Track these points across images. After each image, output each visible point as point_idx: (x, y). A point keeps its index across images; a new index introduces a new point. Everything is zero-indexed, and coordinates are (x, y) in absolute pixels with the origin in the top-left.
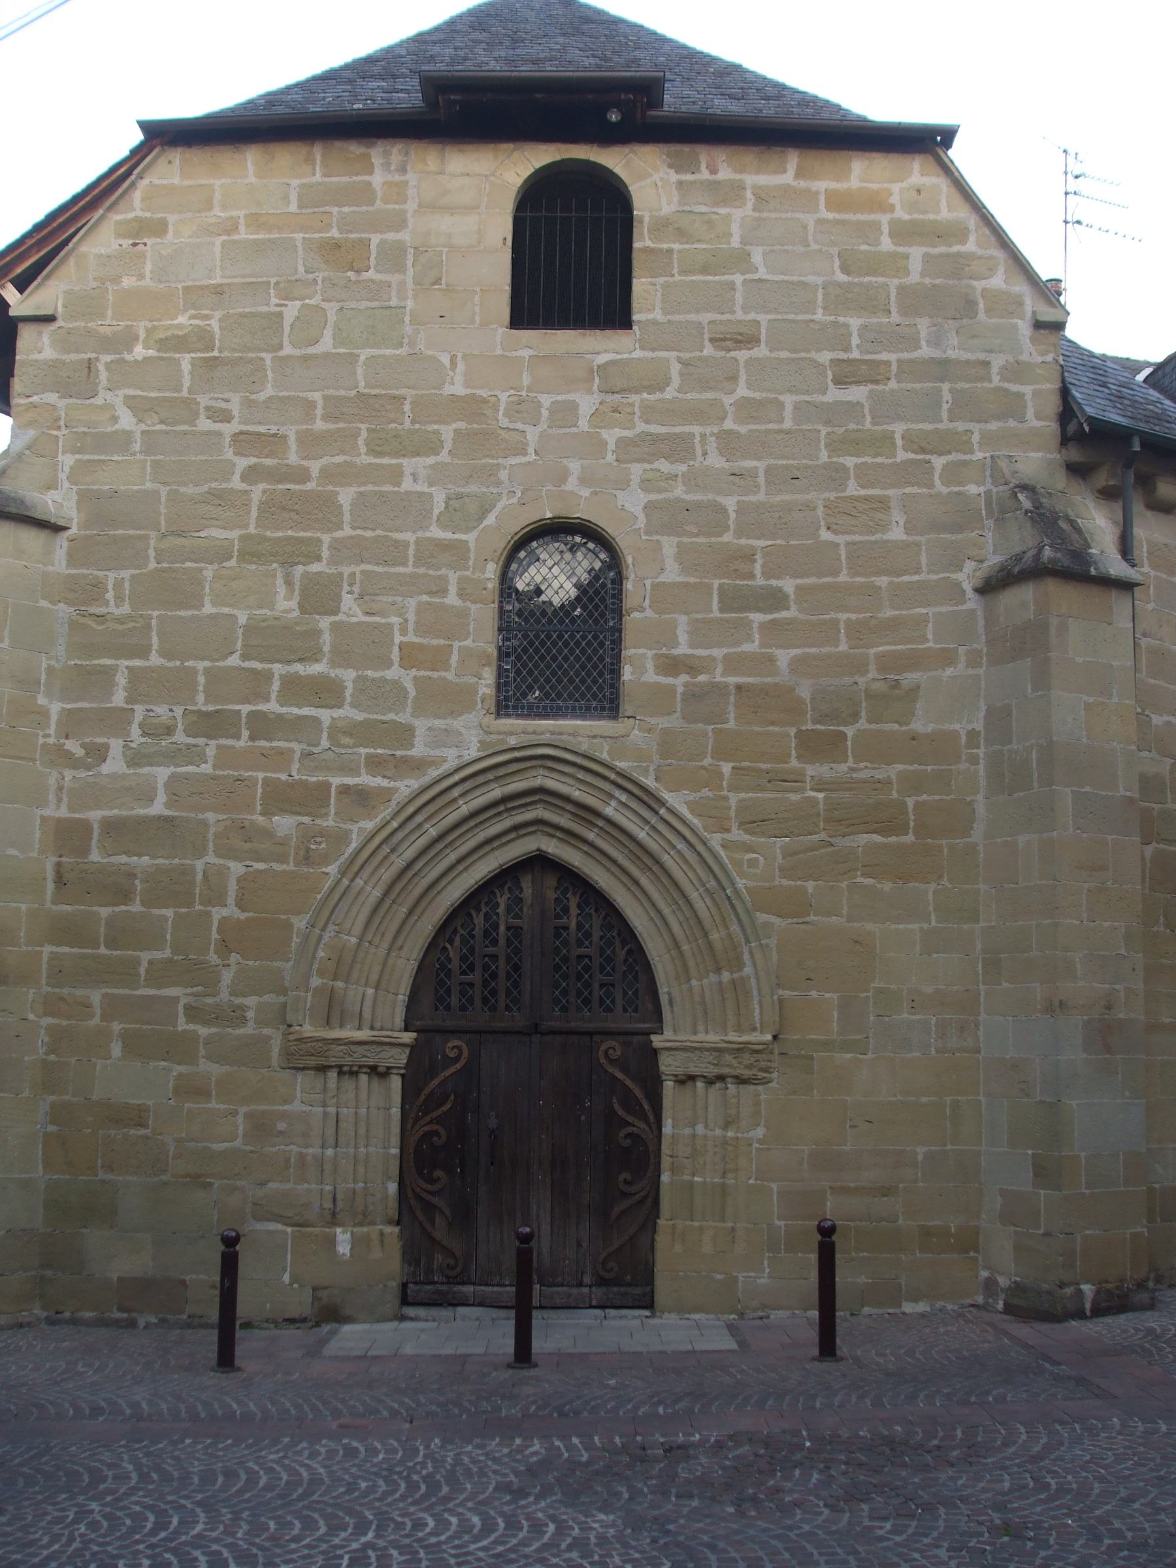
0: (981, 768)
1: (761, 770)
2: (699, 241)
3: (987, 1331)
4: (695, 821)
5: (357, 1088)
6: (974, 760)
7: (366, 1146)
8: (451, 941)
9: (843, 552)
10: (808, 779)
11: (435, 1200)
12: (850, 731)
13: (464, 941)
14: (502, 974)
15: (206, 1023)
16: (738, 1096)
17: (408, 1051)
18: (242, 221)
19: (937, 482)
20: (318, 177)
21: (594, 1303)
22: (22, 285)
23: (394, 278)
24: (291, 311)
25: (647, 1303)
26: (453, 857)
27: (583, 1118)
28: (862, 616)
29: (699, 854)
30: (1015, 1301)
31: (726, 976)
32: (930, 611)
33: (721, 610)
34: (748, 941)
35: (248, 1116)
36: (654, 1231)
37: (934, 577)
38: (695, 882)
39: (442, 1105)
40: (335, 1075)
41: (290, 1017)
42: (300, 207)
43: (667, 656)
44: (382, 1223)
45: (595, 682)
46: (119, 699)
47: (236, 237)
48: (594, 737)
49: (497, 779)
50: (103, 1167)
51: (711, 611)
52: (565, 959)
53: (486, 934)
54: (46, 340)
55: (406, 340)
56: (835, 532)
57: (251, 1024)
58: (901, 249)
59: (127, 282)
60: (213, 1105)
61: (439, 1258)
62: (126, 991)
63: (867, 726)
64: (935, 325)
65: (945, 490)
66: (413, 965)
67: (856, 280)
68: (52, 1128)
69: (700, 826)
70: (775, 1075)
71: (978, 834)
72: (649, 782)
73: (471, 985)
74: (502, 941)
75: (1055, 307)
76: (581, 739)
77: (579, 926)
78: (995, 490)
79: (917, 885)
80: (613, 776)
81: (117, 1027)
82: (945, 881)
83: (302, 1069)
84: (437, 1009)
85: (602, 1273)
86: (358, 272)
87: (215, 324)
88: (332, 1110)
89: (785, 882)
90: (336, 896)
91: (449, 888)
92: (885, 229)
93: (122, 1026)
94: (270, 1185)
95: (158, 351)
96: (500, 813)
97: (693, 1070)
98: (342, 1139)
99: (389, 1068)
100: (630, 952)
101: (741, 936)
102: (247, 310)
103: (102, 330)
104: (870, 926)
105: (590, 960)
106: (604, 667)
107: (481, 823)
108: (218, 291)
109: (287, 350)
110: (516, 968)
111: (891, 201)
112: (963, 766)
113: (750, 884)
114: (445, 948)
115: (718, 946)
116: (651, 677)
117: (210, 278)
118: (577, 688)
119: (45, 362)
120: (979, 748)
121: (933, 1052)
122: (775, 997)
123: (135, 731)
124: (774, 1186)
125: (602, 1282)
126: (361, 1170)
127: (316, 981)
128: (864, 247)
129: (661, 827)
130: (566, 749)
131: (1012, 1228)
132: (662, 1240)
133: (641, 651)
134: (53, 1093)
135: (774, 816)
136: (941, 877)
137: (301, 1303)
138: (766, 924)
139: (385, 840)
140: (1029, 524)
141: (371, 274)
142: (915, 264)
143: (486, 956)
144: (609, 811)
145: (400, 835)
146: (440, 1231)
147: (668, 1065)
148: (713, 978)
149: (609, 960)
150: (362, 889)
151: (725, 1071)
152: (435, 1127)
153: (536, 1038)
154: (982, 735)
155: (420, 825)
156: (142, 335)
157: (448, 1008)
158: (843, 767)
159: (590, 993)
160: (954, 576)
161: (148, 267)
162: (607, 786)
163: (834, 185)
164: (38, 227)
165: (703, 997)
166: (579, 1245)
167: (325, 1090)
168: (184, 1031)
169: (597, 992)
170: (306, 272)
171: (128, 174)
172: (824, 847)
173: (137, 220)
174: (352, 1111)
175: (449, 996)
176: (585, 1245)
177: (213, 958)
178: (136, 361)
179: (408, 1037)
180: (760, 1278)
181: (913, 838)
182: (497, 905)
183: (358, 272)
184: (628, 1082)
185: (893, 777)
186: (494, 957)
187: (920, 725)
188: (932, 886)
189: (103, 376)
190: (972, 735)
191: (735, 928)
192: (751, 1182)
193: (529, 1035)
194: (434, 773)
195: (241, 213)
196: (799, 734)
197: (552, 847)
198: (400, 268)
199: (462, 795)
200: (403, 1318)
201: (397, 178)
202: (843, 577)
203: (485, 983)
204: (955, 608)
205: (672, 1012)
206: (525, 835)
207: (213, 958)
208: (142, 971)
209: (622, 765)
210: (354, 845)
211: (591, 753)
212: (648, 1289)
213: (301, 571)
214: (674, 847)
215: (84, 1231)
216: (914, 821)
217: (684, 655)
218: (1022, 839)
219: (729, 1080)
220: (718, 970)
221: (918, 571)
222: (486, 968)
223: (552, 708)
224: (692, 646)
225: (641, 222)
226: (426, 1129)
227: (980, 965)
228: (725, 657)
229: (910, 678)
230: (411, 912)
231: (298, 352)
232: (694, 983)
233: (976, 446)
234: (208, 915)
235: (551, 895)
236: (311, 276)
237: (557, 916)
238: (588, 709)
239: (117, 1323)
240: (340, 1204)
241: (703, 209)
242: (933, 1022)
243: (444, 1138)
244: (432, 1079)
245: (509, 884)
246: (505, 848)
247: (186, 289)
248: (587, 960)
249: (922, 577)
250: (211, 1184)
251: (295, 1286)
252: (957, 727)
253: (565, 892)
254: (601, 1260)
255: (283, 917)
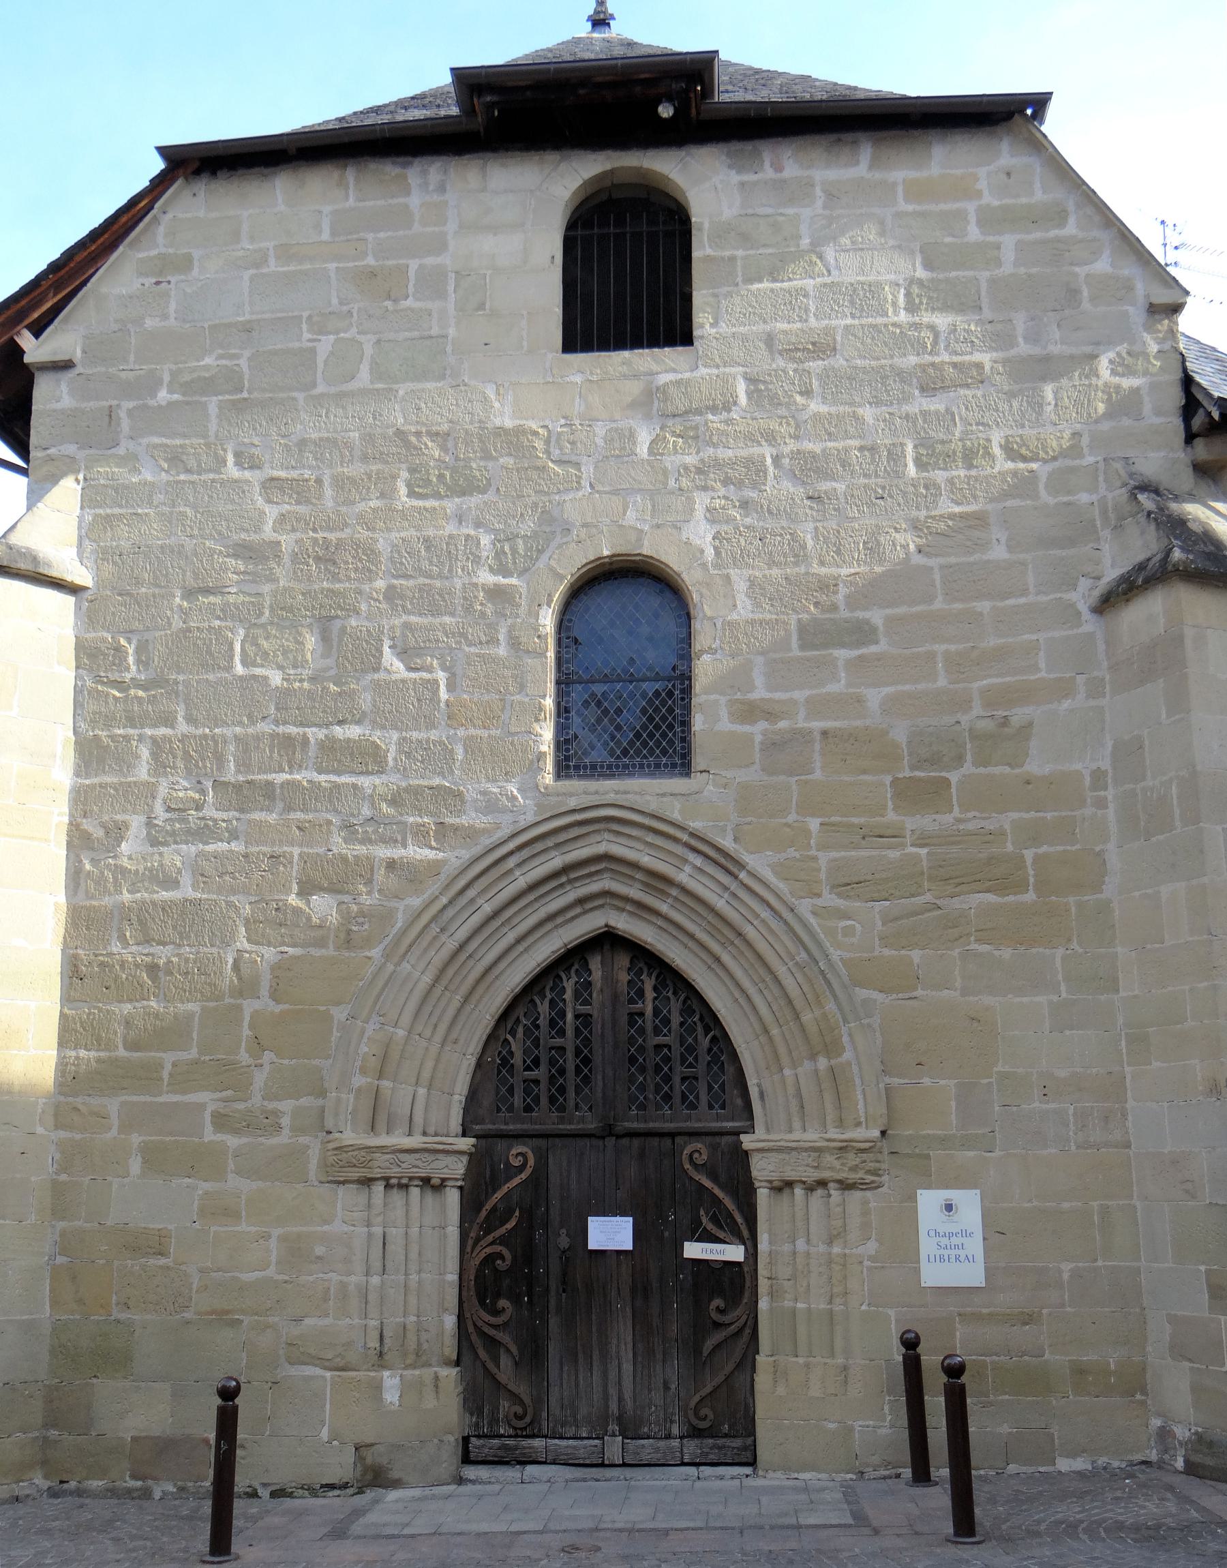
0: (1111, 812)
1: (853, 825)
2: (764, 246)
3: (1168, 1500)
4: (782, 886)
5: (407, 1204)
6: (1101, 804)
7: (420, 1272)
8: (513, 1032)
9: (937, 577)
10: (908, 833)
11: (499, 1335)
12: (954, 777)
13: (527, 1032)
14: (570, 1067)
15: (236, 1132)
16: (843, 1203)
17: (465, 1159)
18: (271, 252)
19: (1043, 493)
20: (351, 202)
21: (687, 1459)
22: (38, 330)
23: (434, 306)
24: (325, 345)
25: (753, 1463)
26: (511, 937)
27: (666, 1234)
28: (961, 646)
29: (786, 923)
30: (1197, 1458)
31: (822, 1063)
32: (1041, 636)
33: (802, 647)
34: (846, 1021)
35: (283, 1239)
36: (754, 1369)
37: (1043, 598)
38: (783, 954)
39: (507, 1221)
40: (382, 1188)
41: (329, 1123)
42: (333, 234)
43: (742, 702)
44: (439, 1365)
45: (664, 735)
46: (142, 772)
47: (265, 270)
48: (663, 795)
49: (557, 845)
50: (117, 1304)
51: (790, 650)
52: (642, 1049)
53: (552, 1023)
54: (64, 388)
55: (448, 372)
56: (928, 555)
57: (286, 1131)
58: (991, 239)
59: (149, 323)
60: (243, 1227)
61: (505, 1405)
62: (148, 1099)
63: (973, 770)
64: (1033, 319)
65: (1051, 501)
66: (471, 1061)
67: (941, 276)
68: (61, 1260)
69: (786, 890)
70: (885, 1178)
71: (1110, 889)
72: (727, 843)
73: (537, 1082)
74: (570, 1032)
75: (1172, 288)
76: (648, 798)
77: (656, 1012)
78: (1110, 496)
79: (1041, 950)
80: (685, 838)
81: (136, 1139)
82: (1075, 945)
83: (343, 1183)
84: (499, 1110)
85: (695, 1422)
86: (395, 301)
87: (243, 363)
88: (378, 1230)
89: (887, 952)
90: (380, 984)
91: (509, 971)
92: (972, 218)
93: (141, 1138)
94: (307, 1321)
95: (184, 395)
96: (562, 885)
97: (790, 1175)
98: (389, 1264)
99: (443, 1180)
100: (714, 1039)
101: (839, 1015)
102: (279, 346)
103: (123, 375)
104: (988, 1000)
105: (670, 1050)
106: (674, 718)
107: (542, 896)
108: (247, 328)
109: (321, 388)
110: (587, 1061)
111: (978, 186)
112: (1088, 811)
113: (847, 955)
114: (506, 1040)
115: (812, 1029)
116: (725, 725)
117: (238, 315)
118: (645, 744)
119: (63, 411)
120: (1106, 789)
121: (1073, 1148)
122: (881, 1086)
123: (159, 809)
124: (892, 1313)
125: (696, 1433)
126: (413, 1300)
127: (359, 1081)
128: (948, 240)
129: (742, 894)
130: (632, 809)
131: (1187, 1364)
132: (762, 1380)
133: (713, 697)
134: (63, 1219)
135: (869, 877)
136: (1069, 940)
137: (341, 1466)
138: (865, 1002)
139: (434, 919)
140: (1153, 527)
141: (409, 303)
142: (1008, 255)
143: (552, 1048)
144: (683, 877)
145: (450, 912)
146: (505, 1371)
147: (762, 1169)
148: (807, 1065)
149: (691, 1049)
150: (409, 974)
151: (826, 1175)
152: (498, 1248)
153: (610, 1142)
154: (1110, 775)
155: (472, 901)
156: (167, 378)
157: (511, 1109)
158: (948, 819)
159: (671, 1088)
160: (1066, 596)
161: (173, 306)
162: (679, 850)
163: (912, 174)
164: (54, 267)
165: (799, 1090)
166: (666, 1387)
167: (369, 1206)
168: (210, 1142)
169: (678, 1087)
170: (341, 303)
171: (150, 208)
172: (929, 911)
173: (162, 257)
174: (402, 1231)
175: (512, 1096)
176: (673, 1386)
177: (244, 1057)
178: (160, 407)
179: (466, 1143)
180: (879, 1427)
181: (1034, 897)
182: (564, 990)
183: (395, 301)
184: (717, 1191)
185: (1007, 827)
186: (562, 1049)
187: (1035, 766)
188: (1060, 952)
189: (125, 424)
190: (1098, 778)
191: (831, 1006)
192: (864, 1307)
193: (603, 1138)
194: (487, 842)
195: (270, 244)
196: (895, 781)
197: (624, 924)
198: (441, 295)
199: (519, 865)
200: (461, 1481)
201: (436, 198)
202: (939, 604)
203: (552, 1080)
204: (1070, 632)
205: (764, 1107)
206: (592, 910)
207: (244, 1057)
208: (165, 1075)
209: (696, 825)
210: (399, 925)
211: (660, 813)
212: (749, 1441)
213: (339, 626)
214: (757, 916)
215: (95, 1381)
216: (1035, 876)
217: (762, 699)
218: (1165, 890)
219: (831, 1185)
220: (813, 1057)
221: (1024, 592)
222: (552, 1062)
223: (617, 767)
224: (770, 689)
225: (700, 230)
226: (488, 1250)
227: (1123, 1043)
228: (807, 701)
229: (1019, 715)
230: (466, 999)
231: (333, 390)
232: (787, 1072)
233: (1086, 450)
234: (239, 1008)
235: (624, 977)
236: (345, 308)
237: (631, 1001)
238: (658, 766)
239: (129, 1492)
240: (387, 1341)
241: (769, 211)
242: (1071, 1111)
243: (508, 1262)
244: (494, 1191)
245: (576, 966)
246: (569, 926)
247: (214, 328)
248: (666, 1050)
249: (1031, 598)
250: (240, 1322)
251: (335, 1443)
252: (1078, 766)
253: (640, 972)
254: (693, 1404)
255: (322, 1008)
